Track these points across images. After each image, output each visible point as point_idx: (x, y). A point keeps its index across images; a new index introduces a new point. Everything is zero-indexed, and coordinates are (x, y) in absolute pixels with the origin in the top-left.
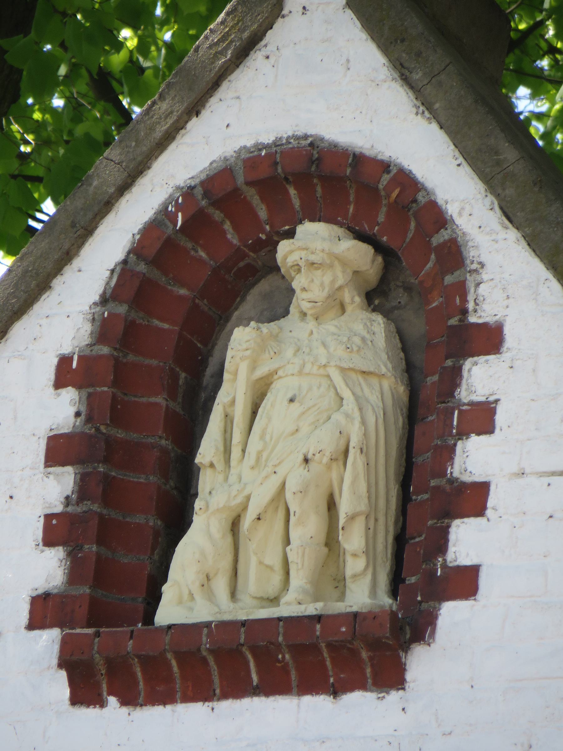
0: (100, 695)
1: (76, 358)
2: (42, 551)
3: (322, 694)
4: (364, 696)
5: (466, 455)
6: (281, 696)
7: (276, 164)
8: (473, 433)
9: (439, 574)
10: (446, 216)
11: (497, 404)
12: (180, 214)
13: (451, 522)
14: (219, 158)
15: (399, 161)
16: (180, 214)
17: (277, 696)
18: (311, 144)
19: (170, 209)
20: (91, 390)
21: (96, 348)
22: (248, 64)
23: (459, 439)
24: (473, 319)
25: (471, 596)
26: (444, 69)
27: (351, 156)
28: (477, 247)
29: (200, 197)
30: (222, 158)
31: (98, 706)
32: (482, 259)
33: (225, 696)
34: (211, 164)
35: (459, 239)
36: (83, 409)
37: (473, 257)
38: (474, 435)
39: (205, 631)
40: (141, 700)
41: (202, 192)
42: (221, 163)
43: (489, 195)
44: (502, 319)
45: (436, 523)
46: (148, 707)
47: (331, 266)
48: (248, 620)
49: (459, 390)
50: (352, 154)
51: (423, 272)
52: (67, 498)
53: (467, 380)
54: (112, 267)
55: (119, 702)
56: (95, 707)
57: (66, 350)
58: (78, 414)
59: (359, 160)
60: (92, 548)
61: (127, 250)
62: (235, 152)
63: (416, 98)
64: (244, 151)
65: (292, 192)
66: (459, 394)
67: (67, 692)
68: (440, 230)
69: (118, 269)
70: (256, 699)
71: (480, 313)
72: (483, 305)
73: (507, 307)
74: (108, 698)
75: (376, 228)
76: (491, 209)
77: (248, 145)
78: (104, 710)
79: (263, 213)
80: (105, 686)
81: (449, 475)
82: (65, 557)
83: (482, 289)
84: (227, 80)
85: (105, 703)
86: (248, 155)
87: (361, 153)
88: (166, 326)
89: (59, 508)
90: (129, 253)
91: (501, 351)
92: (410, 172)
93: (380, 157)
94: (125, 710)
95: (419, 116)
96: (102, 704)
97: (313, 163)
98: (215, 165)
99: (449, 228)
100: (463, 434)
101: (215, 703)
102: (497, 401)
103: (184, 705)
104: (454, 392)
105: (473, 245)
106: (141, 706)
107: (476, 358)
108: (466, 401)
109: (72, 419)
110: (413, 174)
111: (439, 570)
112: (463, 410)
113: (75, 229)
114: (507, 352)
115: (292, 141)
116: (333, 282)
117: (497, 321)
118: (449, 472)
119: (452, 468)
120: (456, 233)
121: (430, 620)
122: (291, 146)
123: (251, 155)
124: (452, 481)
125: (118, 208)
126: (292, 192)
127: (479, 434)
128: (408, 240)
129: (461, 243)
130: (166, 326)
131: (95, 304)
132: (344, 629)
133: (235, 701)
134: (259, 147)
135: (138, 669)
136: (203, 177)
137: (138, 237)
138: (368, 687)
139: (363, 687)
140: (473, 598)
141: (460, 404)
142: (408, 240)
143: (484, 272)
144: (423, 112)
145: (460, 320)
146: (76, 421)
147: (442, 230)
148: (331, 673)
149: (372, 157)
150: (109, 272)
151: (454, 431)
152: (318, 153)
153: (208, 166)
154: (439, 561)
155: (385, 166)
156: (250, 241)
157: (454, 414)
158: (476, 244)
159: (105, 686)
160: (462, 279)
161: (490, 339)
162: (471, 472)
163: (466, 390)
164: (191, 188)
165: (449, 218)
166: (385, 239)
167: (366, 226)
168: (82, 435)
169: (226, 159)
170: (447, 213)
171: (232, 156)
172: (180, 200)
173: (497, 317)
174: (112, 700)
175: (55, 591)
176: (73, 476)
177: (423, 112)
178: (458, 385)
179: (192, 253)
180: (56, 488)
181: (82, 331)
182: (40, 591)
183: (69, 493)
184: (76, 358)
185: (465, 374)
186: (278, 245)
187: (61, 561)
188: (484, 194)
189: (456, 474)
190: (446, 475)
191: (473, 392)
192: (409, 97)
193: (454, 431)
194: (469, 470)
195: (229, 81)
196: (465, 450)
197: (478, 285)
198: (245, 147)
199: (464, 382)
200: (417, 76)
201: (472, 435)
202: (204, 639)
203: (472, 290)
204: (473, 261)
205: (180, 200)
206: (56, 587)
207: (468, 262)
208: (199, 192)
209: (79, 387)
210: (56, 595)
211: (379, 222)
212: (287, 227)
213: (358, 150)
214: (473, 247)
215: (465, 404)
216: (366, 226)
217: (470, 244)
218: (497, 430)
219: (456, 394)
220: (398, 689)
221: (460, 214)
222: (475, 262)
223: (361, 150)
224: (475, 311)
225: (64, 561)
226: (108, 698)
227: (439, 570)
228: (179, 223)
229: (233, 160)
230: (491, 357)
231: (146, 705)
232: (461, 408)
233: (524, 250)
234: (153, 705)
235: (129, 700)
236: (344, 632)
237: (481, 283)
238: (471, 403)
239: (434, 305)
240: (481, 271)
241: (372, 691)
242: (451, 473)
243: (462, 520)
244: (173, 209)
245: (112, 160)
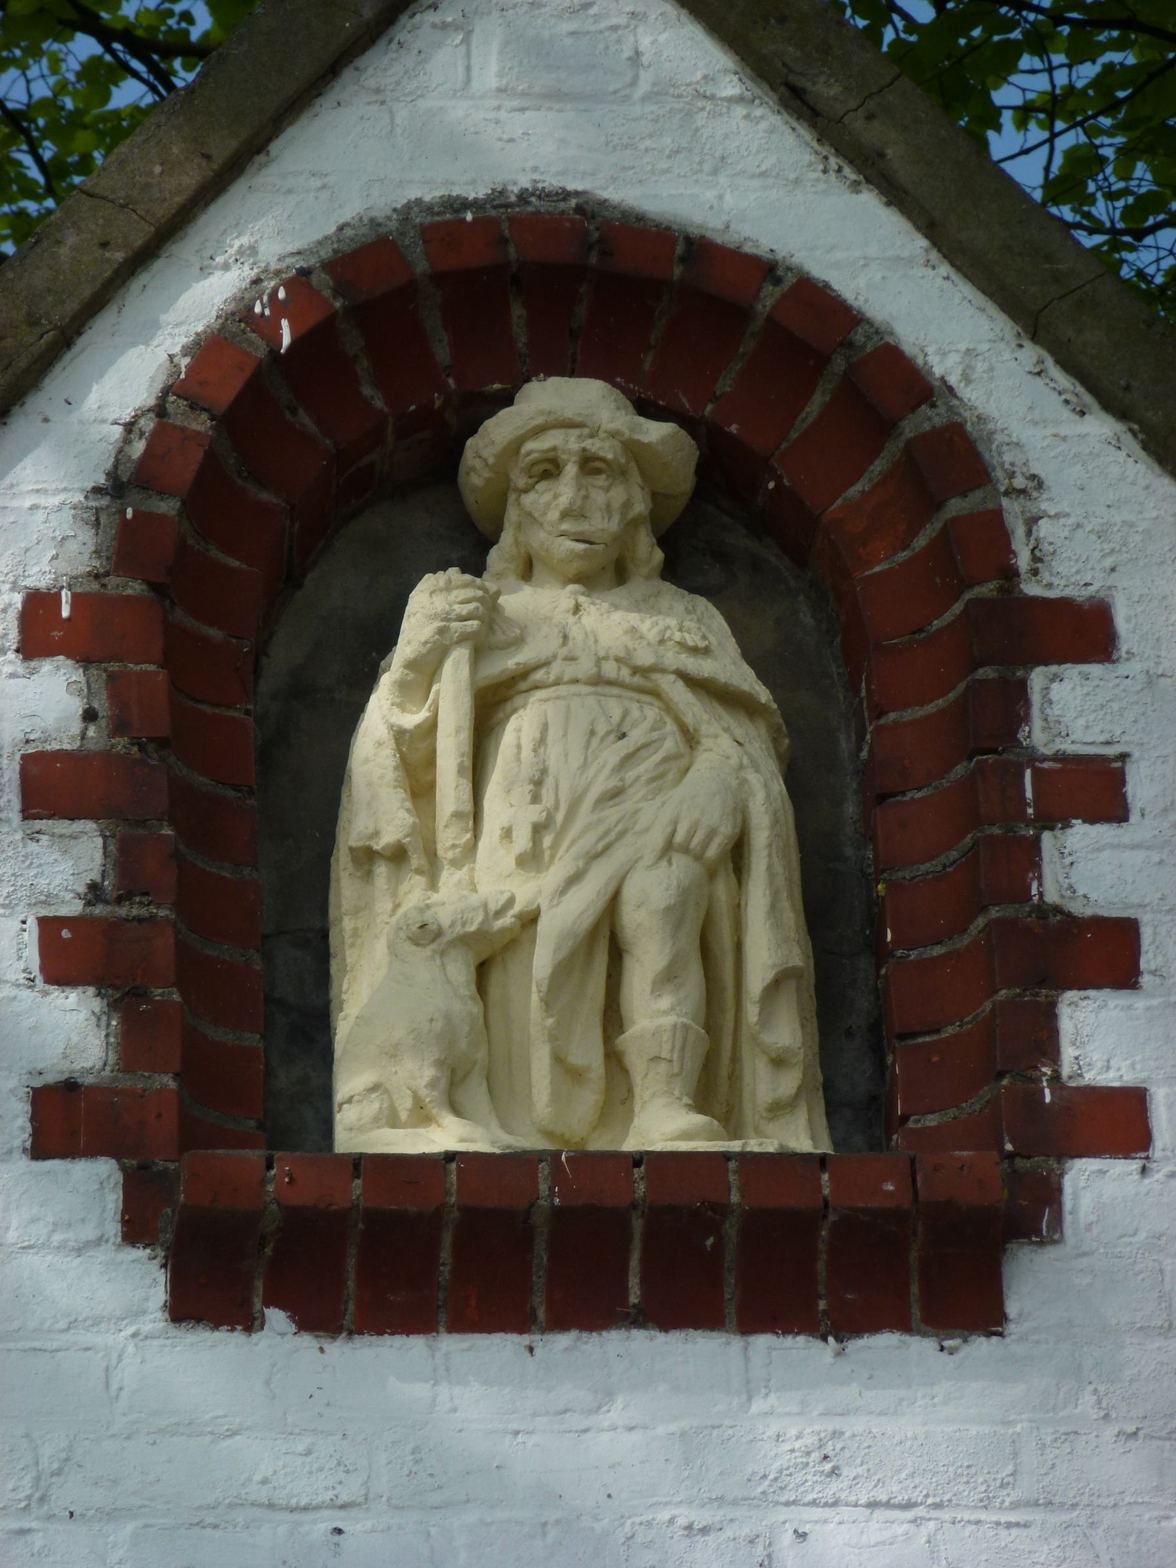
0: (247, 1303)
1: (65, 596)
2: (46, 994)
3: (798, 1334)
4: (904, 1342)
5: (1068, 861)
6: (699, 1332)
7: (505, 241)
8: (1077, 818)
9: (1048, 1099)
10: (929, 378)
11: (1124, 762)
12: (285, 323)
13: (1058, 996)
14: (357, 219)
15: (795, 260)
16: (285, 323)
17: (692, 1332)
18: (579, 209)
19: (258, 309)
20: (114, 667)
21: (112, 581)
22: (402, 36)
23: (1045, 828)
24: (1032, 589)
25: (1137, 1151)
26: (891, 84)
27: (681, 241)
28: (1017, 444)
29: (327, 293)
30: (365, 220)
31: (239, 1328)
32: (1036, 469)
33: (559, 1323)
34: (341, 229)
35: (969, 427)
36: (101, 704)
37: (1012, 464)
38: (1080, 821)
39: (544, 1169)
40: (348, 1321)
41: (331, 283)
42: (364, 230)
43: (1027, 344)
44: (1102, 594)
45: (1019, 995)
46: (367, 1339)
47: (624, 473)
48: (647, 1152)
49: (1027, 729)
50: (681, 238)
51: (839, 501)
52: (93, 887)
53: (1042, 711)
54: (126, 415)
55: (294, 1321)
56: (233, 1330)
57: (40, 577)
58: (89, 716)
59: (700, 251)
60: (171, 994)
61: (158, 386)
62: (395, 210)
63: (819, 140)
64: (416, 209)
65: (517, 311)
66: (1029, 737)
67: (159, 1294)
68: (918, 405)
69: (148, 424)
70: (638, 1335)
71: (1046, 577)
72: (1054, 563)
73: (1113, 570)
74: (266, 1311)
75: (709, 407)
76: (1039, 374)
77: (427, 199)
78: (255, 1337)
79: (442, 352)
80: (259, 1285)
81: (1036, 899)
82: (106, 1010)
83: (1044, 529)
84: (352, 66)
85: (257, 1323)
86: (429, 219)
87: (702, 237)
88: (235, 563)
89: (73, 908)
90: (166, 391)
91: (1114, 657)
92: (827, 285)
93: (748, 249)
94: (307, 1341)
95: (833, 176)
96: (250, 1323)
97: (591, 247)
98: (349, 232)
99: (939, 403)
100: (1054, 817)
101: (538, 1337)
102: (1124, 757)
103: (456, 1337)
104: (1017, 732)
105: (1007, 440)
106: (351, 1333)
107: (1054, 668)
108: (1048, 751)
109: (76, 726)
110: (834, 291)
111: (1047, 1092)
112: (1043, 769)
113: (38, 330)
114: (1128, 659)
115: (533, 199)
116: (627, 505)
117: (1091, 597)
118: (1034, 891)
119: (1040, 885)
120: (959, 414)
121: (1050, 1194)
122: (530, 209)
123: (437, 218)
124: (1044, 911)
125: (124, 298)
126: (517, 311)
127: (1092, 820)
128: (794, 435)
129: (975, 435)
130: (235, 563)
131: (97, 490)
132: (890, 1187)
133: (585, 1335)
134: (456, 205)
135: (353, 1251)
136: (326, 253)
137: (185, 362)
138: (914, 1325)
139: (904, 1326)
140: (1143, 1155)
141: (1033, 758)
142: (794, 435)
143: (1045, 496)
144: (840, 170)
145: (1001, 589)
146: (86, 729)
147: (923, 407)
148: (821, 1290)
149: (732, 246)
150: (118, 431)
151: (1030, 811)
152: (597, 229)
153: (334, 233)
154: (1045, 1074)
155: (768, 269)
156: (413, 408)
157: (1023, 777)
158: (1014, 439)
159: (259, 1285)
160: (990, 506)
161: (1085, 632)
162: (1085, 896)
163: (1044, 729)
164: (304, 273)
165: (937, 384)
166: (734, 428)
167: (684, 400)
168: (106, 756)
169: (374, 223)
170: (932, 374)
171: (389, 218)
172: (282, 294)
173: (1091, 590)
174: (276, 1317)
175: (89, 1080)
176: (100, 841)
177: (840, 170)
178: (1026, 719)
179: (288, 415)
180: (66, 865)
181: (73, 547)
182: (51, 1078)
183: (95, 875)
184: (65, 596)
185: (1036, 698)
186: (492, 414)
187: (99, 1019)
188: (1014, 344)
189: (1052, 897)
190: (1030, 898)
191: (1064, 734)
192: (798, 136)
193: (1030, 811)
194: (1080, 892)
195: (357, 69)
196: (1066, 851)
197: (1032, 521)
198: (419, 201)
199: (1035, 712)
200: (826, 89)
201: (1073, 821)
202: (543, 1188)
203: (1019, 531)
204: (1014, 472)
205: (282, 294)
206: (89, 1071)
207: (999, 474)
208: (322, 281)
209: (85, 660)
210: (91, 1089)
211: (718, 393)
212: (497, 386)
213: (695, 232)
214: (1008, 444)
215: (1045, 758)
216: (684, 400)
217: (999, 438)
218: (1134, 817)
219: (1020, 736)
220: (990, 1334)
221: (966, 378)
222: (1018, 474)
223: (703, 232)
224: (1035, 572)
225: (104, 1018)
226: (266, 1311)
227: (1047, 1092)
228: (286, 340)
229: (393, 225)
230: (1095, 669)
231: (361, 1333)
232: (1038, 764)
233: (1131, 460)
234: (380, 1333)
235: (320, 1318)
236: (890, 1193)
237: (1042, 518)
238: (1061, 757)
239: (877, 569)
240: (1035, 494)
241: (924, 1335)
242: (1041, 894)
243: (1083, 993)
244: (267, 312)
245: (104, 198)
